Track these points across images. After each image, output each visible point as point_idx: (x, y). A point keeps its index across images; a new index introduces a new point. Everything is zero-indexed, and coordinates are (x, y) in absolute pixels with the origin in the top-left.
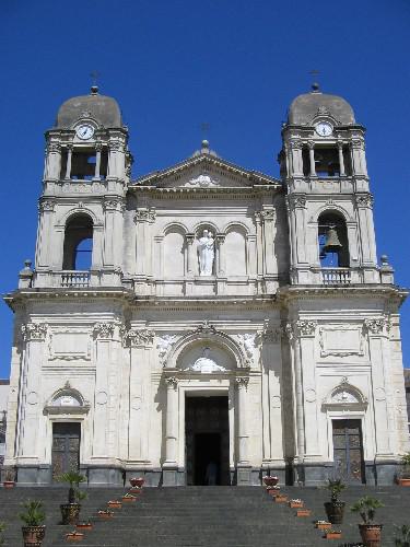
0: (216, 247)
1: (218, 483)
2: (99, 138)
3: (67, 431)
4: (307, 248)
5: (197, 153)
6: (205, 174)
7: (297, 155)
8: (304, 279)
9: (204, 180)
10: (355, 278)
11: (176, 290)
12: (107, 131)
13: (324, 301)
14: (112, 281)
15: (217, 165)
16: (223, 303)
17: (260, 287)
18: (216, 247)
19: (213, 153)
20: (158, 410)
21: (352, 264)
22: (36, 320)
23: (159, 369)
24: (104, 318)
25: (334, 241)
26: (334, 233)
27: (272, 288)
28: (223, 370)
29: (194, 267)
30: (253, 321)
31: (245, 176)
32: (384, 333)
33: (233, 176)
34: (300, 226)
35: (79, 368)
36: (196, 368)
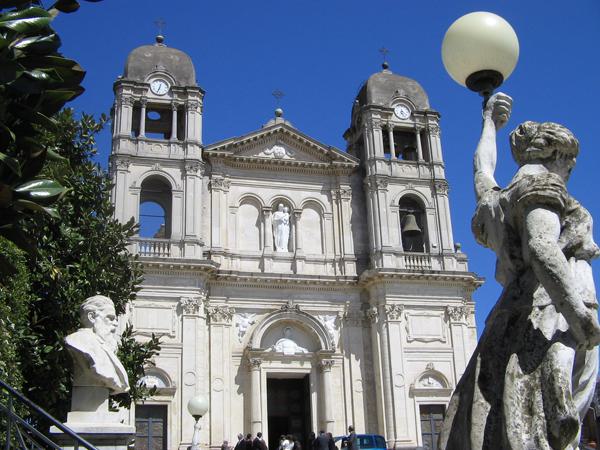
0: (293, 221)
2: (175, 96)
4: (389, 232)
5: (272, 123)
6: (280, 145)
7: (378, 135)
8: (389, 262)
9: (279, 151)
10: (175, 252)
11: (252, 267)
12: (185, 89)
13: (411, 287)
14: (194, 253)
15: (294, 137)
16: (305, 282)
17: (338, 268)
18: (293, 221)
19: (287, 124)
20: (239, 392)
21: (432, 250)
22: (390, 301)
23: (241, 347)
24: (190, 294)
25: (413, 226)
26: (413, 218)
27: (351, 270)
28: (306, 352)
30: (334, 302)
31: (321, 151)
32: (463, 320)
33: (307, 148)
36: (279, 347)
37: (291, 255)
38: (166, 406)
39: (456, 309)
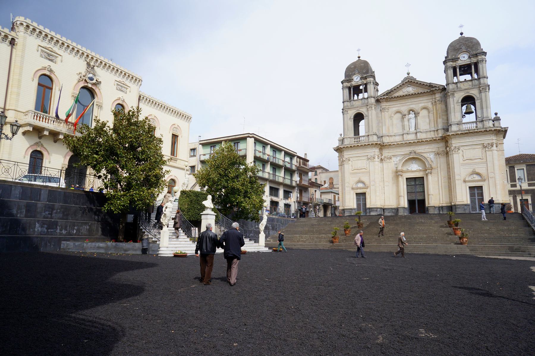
0: (416, 117)
1: (420, 212)
3: (361, 196)
29: (407, 129)
34: (452, 106)
35: (363, 173)
37: (415, 131)
38: (482, 187)
39: (489, 144)
